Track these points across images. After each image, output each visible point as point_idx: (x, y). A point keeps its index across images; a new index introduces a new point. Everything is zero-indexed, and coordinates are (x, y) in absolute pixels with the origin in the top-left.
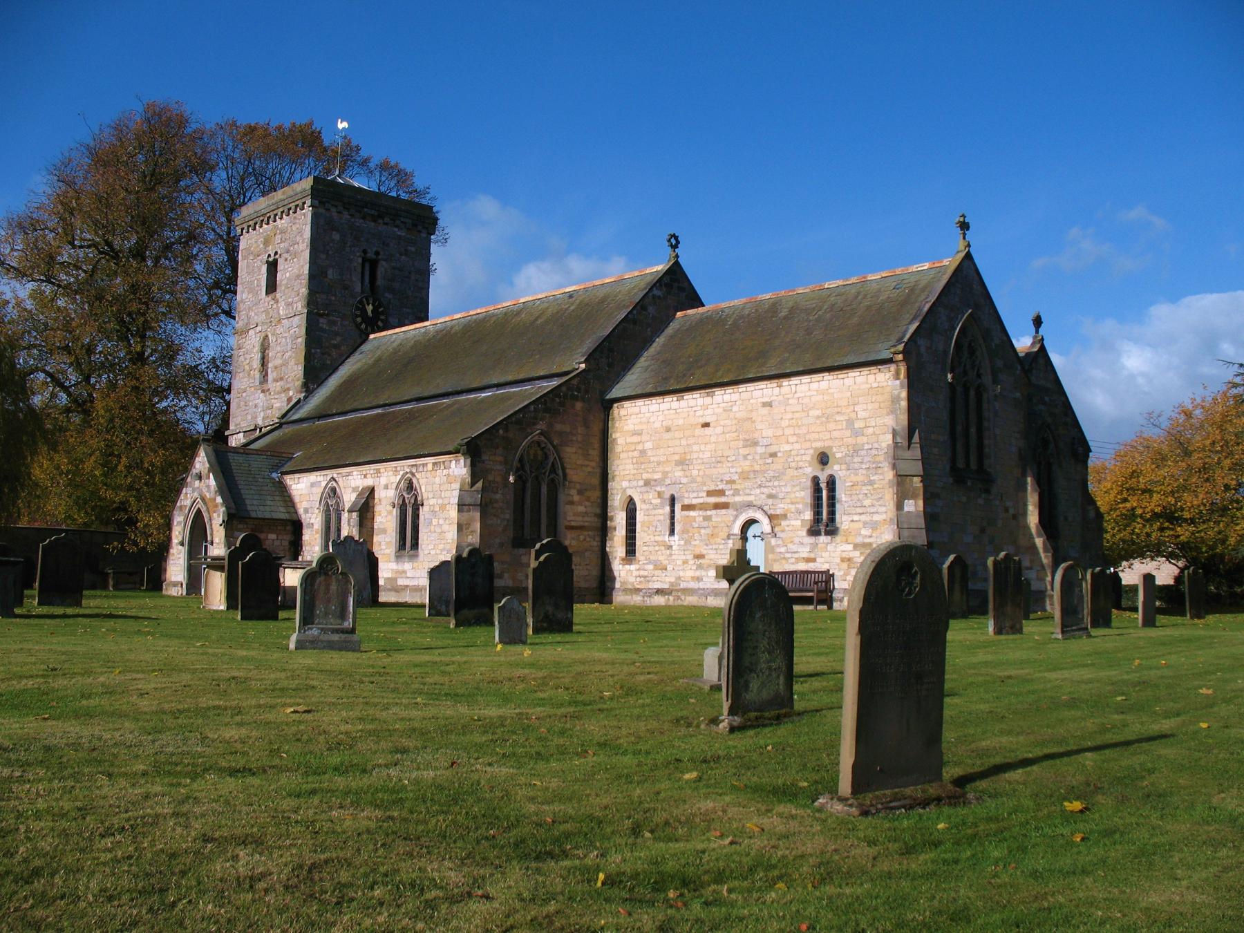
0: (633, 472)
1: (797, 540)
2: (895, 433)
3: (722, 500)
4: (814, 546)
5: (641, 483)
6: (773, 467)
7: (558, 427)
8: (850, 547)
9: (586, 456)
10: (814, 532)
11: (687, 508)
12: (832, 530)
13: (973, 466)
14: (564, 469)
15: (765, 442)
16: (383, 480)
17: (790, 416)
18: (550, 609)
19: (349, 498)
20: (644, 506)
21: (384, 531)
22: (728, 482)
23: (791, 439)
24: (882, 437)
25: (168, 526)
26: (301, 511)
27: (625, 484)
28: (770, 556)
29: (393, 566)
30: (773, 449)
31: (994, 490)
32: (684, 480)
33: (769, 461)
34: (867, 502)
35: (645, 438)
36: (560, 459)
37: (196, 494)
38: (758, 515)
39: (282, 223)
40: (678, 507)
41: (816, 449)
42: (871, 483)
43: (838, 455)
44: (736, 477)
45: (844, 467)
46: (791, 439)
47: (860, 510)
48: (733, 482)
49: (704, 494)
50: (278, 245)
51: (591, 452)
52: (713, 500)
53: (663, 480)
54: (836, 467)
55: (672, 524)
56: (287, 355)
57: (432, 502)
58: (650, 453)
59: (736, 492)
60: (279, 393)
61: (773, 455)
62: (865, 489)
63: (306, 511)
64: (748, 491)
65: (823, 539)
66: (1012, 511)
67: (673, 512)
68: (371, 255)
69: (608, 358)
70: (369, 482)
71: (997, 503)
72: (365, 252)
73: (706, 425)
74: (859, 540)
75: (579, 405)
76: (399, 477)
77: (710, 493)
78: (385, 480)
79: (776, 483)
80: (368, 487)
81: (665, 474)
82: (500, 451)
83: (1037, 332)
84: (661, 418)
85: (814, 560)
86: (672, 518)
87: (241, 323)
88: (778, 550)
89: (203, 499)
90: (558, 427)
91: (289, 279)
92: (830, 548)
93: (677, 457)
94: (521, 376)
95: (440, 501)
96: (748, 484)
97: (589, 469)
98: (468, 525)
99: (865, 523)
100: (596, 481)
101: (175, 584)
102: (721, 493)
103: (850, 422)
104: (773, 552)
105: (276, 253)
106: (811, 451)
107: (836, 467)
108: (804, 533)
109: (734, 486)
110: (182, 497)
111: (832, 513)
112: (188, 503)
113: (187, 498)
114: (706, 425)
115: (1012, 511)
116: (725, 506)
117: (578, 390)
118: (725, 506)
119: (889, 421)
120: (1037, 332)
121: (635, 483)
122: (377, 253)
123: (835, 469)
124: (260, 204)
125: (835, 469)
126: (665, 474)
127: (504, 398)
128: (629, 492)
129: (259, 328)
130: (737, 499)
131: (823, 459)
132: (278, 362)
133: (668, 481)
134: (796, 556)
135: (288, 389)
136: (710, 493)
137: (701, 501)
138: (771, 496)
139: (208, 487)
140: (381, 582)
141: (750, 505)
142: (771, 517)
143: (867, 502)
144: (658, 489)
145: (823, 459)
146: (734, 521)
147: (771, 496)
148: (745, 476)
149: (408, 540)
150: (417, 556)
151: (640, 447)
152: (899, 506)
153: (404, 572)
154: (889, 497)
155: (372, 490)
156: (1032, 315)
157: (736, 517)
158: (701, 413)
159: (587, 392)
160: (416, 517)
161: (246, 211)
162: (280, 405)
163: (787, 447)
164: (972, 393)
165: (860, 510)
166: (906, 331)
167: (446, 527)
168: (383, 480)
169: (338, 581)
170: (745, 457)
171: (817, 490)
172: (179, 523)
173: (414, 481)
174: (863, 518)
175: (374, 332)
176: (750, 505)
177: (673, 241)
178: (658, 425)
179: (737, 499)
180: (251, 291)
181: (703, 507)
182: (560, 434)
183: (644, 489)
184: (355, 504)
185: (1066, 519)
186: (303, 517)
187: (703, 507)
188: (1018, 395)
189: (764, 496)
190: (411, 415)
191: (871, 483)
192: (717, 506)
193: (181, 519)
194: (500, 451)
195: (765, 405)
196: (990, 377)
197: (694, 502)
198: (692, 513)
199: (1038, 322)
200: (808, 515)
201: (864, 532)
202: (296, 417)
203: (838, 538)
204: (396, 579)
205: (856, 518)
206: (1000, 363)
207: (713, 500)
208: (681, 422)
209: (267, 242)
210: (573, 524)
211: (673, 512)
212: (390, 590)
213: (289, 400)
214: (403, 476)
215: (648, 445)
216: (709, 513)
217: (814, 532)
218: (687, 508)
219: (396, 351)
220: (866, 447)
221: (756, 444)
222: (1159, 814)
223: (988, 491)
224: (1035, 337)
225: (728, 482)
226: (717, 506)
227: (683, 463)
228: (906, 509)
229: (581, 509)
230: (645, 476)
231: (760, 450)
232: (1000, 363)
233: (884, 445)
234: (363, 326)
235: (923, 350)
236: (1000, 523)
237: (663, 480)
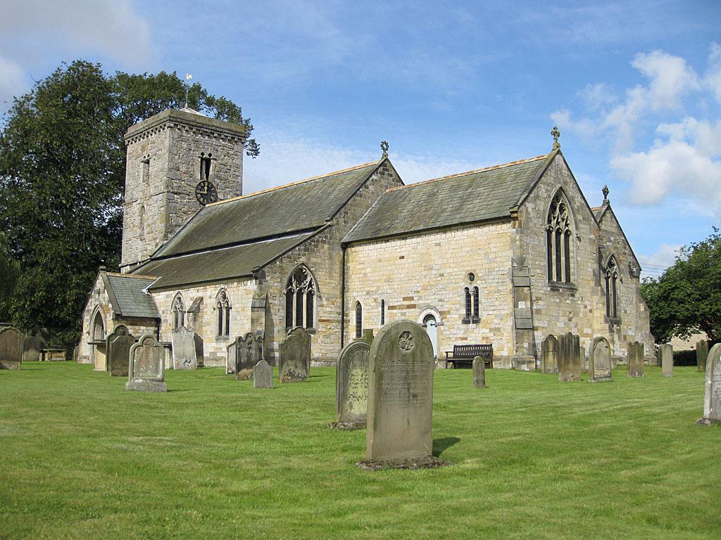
0: (359, 286)
1: (456, 327)
2: (513, 261)
3: (413, 303)
4: (466, 331)
5: (364, 293)
6: (442, 282)
7: (313, 260)
8: (488, 330)
9: (331, 277)
10: (466, 322)
11: (391, 308)
12: (477, 322)
13: (563, 280)
14: (317, 285)
15: (437, 267)
16: (208, 293)
17: (452, 251)
18: (292, 368)
19: (188, 304)
20: (366, 308)
21: (208, 324)
22: (415, 292)
23: (452, 265)
24: (505, 263)
25: (703, 403)
26: (160, 312)
27: (355, 294)
28: (441, 337)
29: (214, 345)
30: (441, 272)
31: (577, 295)
32: (390, 291)
33: (440, 278)
34: (497, 303)
35: (366, 265)
36: (315, 279)
37: (97, 303)
38: (433, 312)
39: (153, 137)
40: (386, 307)
41: (467, 271)
42: (499, 291)
43: (480, 275)
44: (420, 289)
45: (483, 282)
46: (452, 265)
47: (492, 308)
48: (419, 292)
49: (402, 299)
50: (150, 151)
51: (334, 274)
52: (407, 303)
53: (377, 291)
54: (479, 282)
55: (383, 318)
56: (155, 218)
57: (237, 306)
58: (369, 275)
59: (420, 298)
60: (150, 241)
61: (442, 275)
62: (496, 295)
63: (163, 312)
64: (427, 297)
65: (471, 325)
66: (589, 308)
67: (383, 310)
68: (206, 156)
69: (344, 217)
70: (200, 294)
71: (579, 302)
72: (203, 154)
73: (402, 257)
74: (493, 326)
75: (326, 246)
76: (217, 291)
77: (405, 299)
78: (210, 294)
79: (444, 292)
80: (200, 297)
81: (378, 287)
82: (278, 275)
83: (605, 198)
84: (376, 254)
85: (466, 339)
86: (383, 314)
87: (128, 198)
88: (446, 333)
89: (101, 305)
90: (313, 260)
91: (156, 172)
92: (475, 331)
93: (385, 277)
94: (188, 250)
95: (241, 305)
96: (427, 293)
97: (334, 285)
98: (258, 320)
99: (496, 316)
100: (338, 292)
101: (85, 358)
102: (412, 299)
103: (487, 254)
104: (442, 334)
105: (149, 155)
106: (464, 273)
107: (479, 282)
108: (460, 322)
109: (419, 294)
110: (89, 304)
111: (477, 310)
112: (92, 308)
113: (91, 305)
114: (402, 257)
115: (589, 308)
116: (414, 306)
117: (326, 237)
118: (414, 306)
119: (510, 253)
120: (605, 198)
121: (360, 293)
122: (210, 155)
123: (477, 283)
124: (140, 124)
125: (477, 283)
126: (378, 287)
127: (284, 241)
128: (357, 299)
129: (139, 201)
130: (421, 302)
131: (471, 276)
132: (150, 221)
133: (380, 292)
134: (456, 336)
135: (156, 238)
136: (405, 299)
137: (399, 303)
138: (440, 300)
139: (104, 298)
140: (205, 355)
141: (428, 307)
142: (441, 313)
143: (497, 303)
144: (374, 297)
145: (471, 276)
146: (419, 316)
147: (440, 300)
148: (425, 288)
149: (223, 328)
150: (228, 339)
151: (363, 271)
152: (516, 305)
153: (221, 349)
154: (510, 299)
155: (202, 299)
156: (603, 187)
157: (421, 313)
158: (399, 250)
159: (331, 238)
160: (228, 315)
161: (131, 130)
162: (151, 248)
163: (450, 270)
164: (562, 236)
165: (492, 308)
166: (519, 199)
167: (245, 321)
168: (208, 293)
169: (153, 351)
170: (425, 276)
171: (468, 296)
172: (87, 320)
173: (227, 293)
174: (495, 312)
175: (208, 203)
176: (428, 307)
177: (384, 146)
178: (373, 258)
179: (421, 302)
180: (133, 177)
181: (401, 307)
182: (314, 264)
183: (367, 297)
184: (191, 308)
185: (626, 312)
186: (162, 315)
187: (401, 307)
188: (592, 236)
189: (437, 300)
190: (227, 253)
191: (499, 291)
192: (409, 307)
193: (88, 317)
194: (278, 275)
195: (436, 245)
196: (574, 226)
197: (396, 304)
198: (394, 311)
199: (606, 192)
200: (463, 311)
201: (495, 321)
202: (159, 256)
203: (480, 325)
204: (216, 353)
205: (491, 313)
206: (580, 217)
207: (407, 303)
208: (387, 256)
209: (143, 149)
210: (323, 318)
211: (383, 310)
212: (213, 359)
213: (157, 245)
214: (220, 290)
215: (368, 270)
216: (404, 311)
217: (466, 322)
218: (391, 308)
219: (222, 213)
220: (496, 269)
221: (431, 269)
222: (30, 332)
223: (573, 295)
224: (604, 201)
225: (415, 292)
226: (409, 307)
227: (388, 280)
228: (520, 307)
229: (328, 309)
230: (367, 289)
231: (434, 272)
232: (580, 217)
233: (507, 268)
234: (202, 199)
235: (530, 210)
236: (581, 315)
237: (377, 291)
